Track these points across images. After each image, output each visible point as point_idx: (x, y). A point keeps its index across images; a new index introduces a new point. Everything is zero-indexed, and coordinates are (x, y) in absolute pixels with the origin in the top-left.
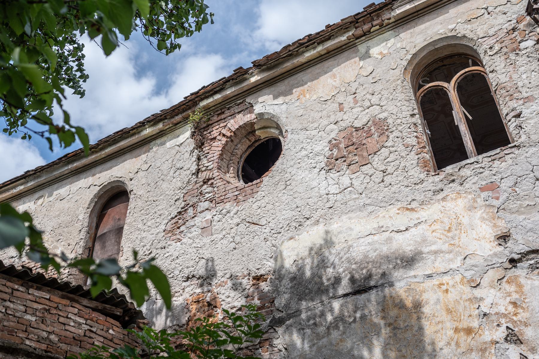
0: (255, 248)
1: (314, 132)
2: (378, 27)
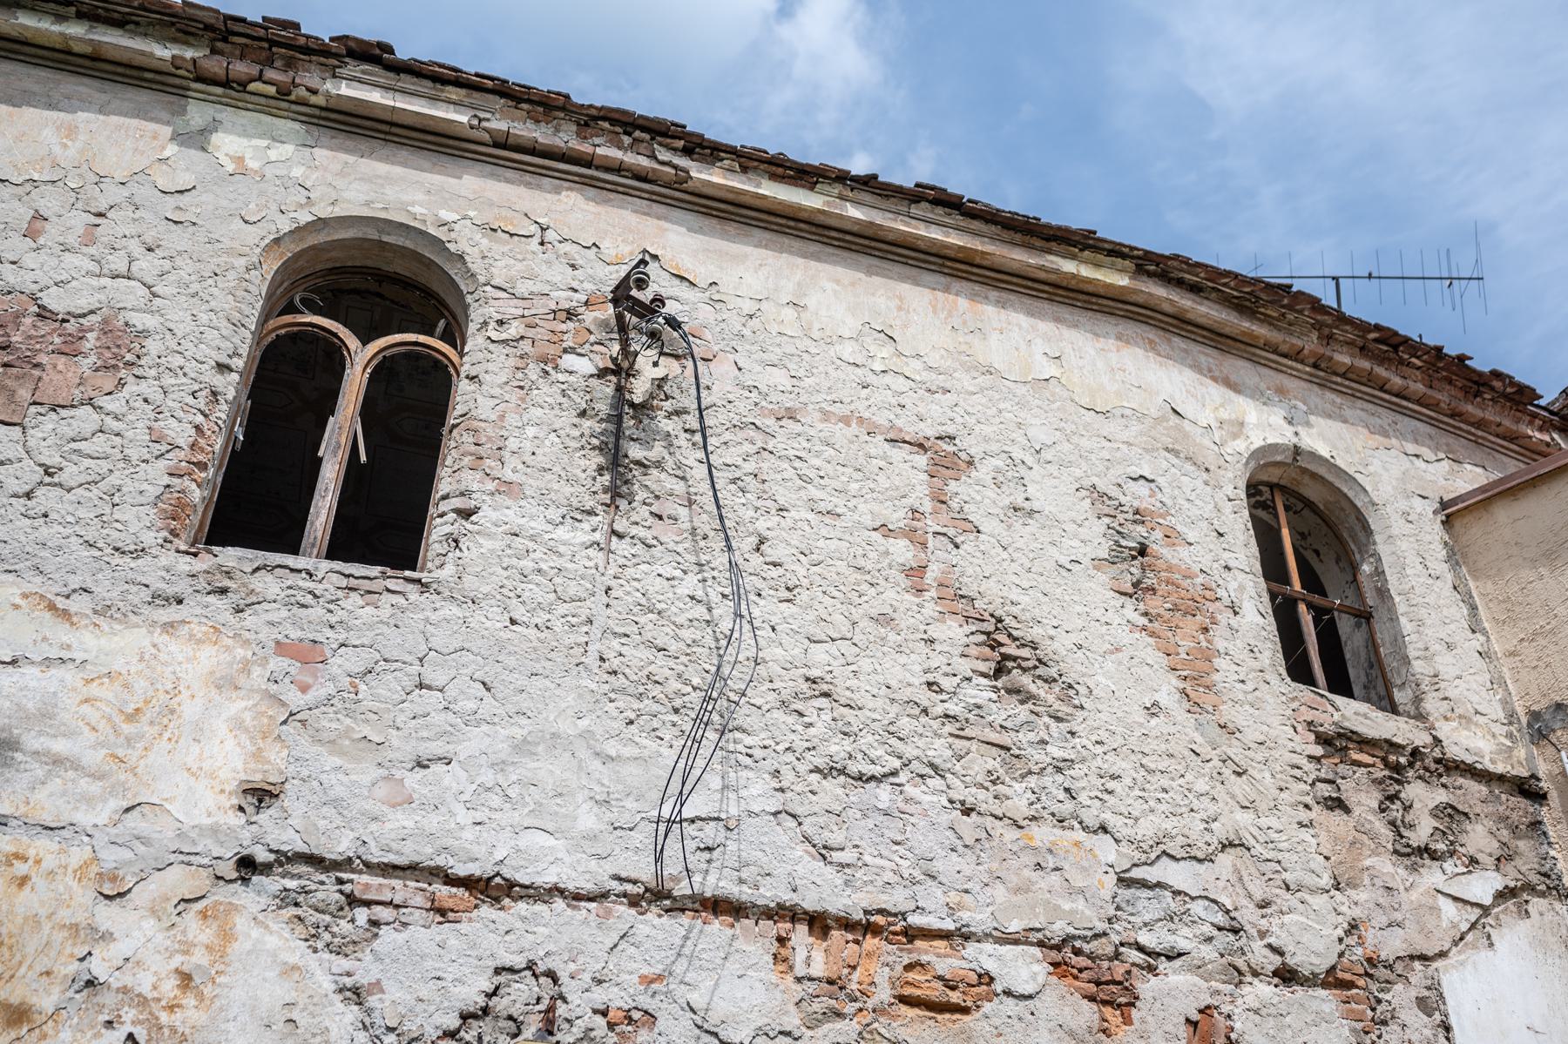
2: (272, 90)
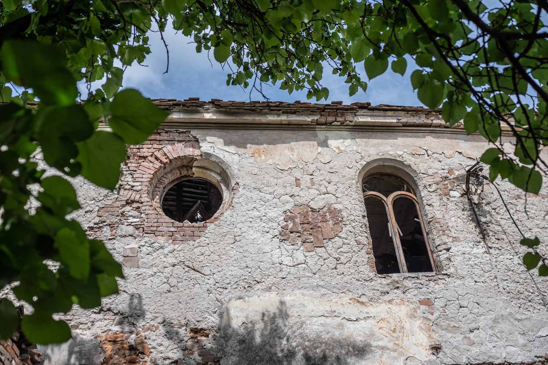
0: (196, 297)
1: (269, 197)
2: (339, 123)
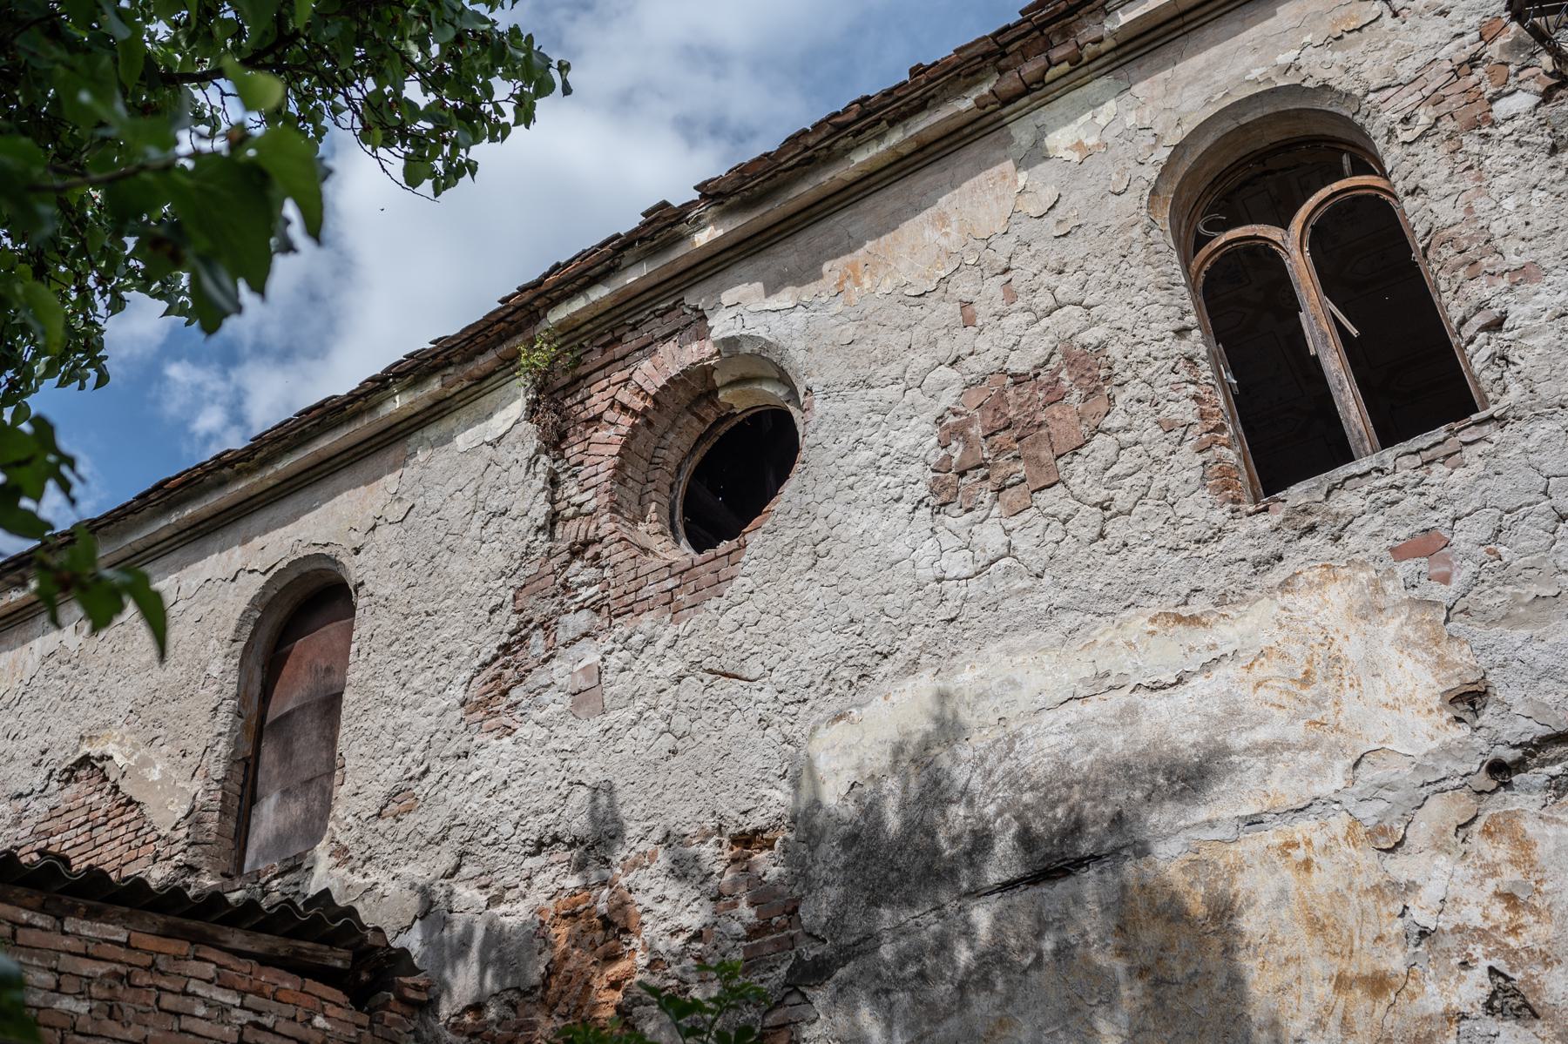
0: (734, 748)
1: (892, 392)
2: (1065, 66)
